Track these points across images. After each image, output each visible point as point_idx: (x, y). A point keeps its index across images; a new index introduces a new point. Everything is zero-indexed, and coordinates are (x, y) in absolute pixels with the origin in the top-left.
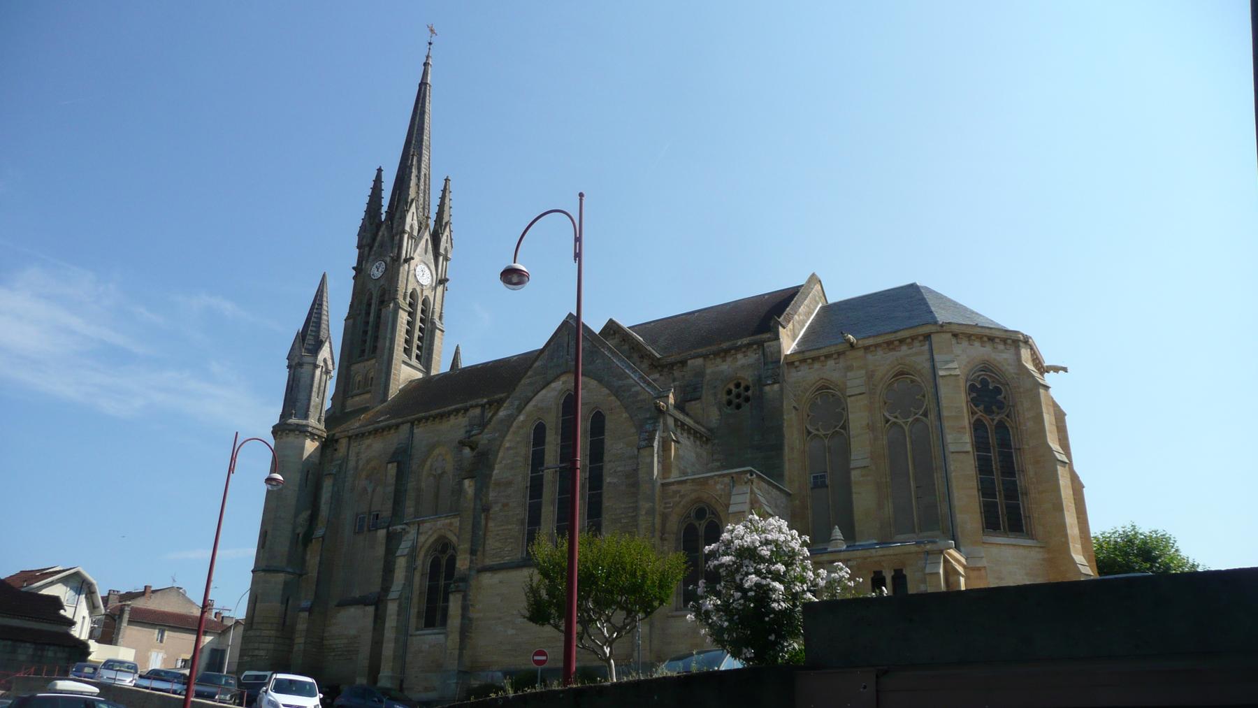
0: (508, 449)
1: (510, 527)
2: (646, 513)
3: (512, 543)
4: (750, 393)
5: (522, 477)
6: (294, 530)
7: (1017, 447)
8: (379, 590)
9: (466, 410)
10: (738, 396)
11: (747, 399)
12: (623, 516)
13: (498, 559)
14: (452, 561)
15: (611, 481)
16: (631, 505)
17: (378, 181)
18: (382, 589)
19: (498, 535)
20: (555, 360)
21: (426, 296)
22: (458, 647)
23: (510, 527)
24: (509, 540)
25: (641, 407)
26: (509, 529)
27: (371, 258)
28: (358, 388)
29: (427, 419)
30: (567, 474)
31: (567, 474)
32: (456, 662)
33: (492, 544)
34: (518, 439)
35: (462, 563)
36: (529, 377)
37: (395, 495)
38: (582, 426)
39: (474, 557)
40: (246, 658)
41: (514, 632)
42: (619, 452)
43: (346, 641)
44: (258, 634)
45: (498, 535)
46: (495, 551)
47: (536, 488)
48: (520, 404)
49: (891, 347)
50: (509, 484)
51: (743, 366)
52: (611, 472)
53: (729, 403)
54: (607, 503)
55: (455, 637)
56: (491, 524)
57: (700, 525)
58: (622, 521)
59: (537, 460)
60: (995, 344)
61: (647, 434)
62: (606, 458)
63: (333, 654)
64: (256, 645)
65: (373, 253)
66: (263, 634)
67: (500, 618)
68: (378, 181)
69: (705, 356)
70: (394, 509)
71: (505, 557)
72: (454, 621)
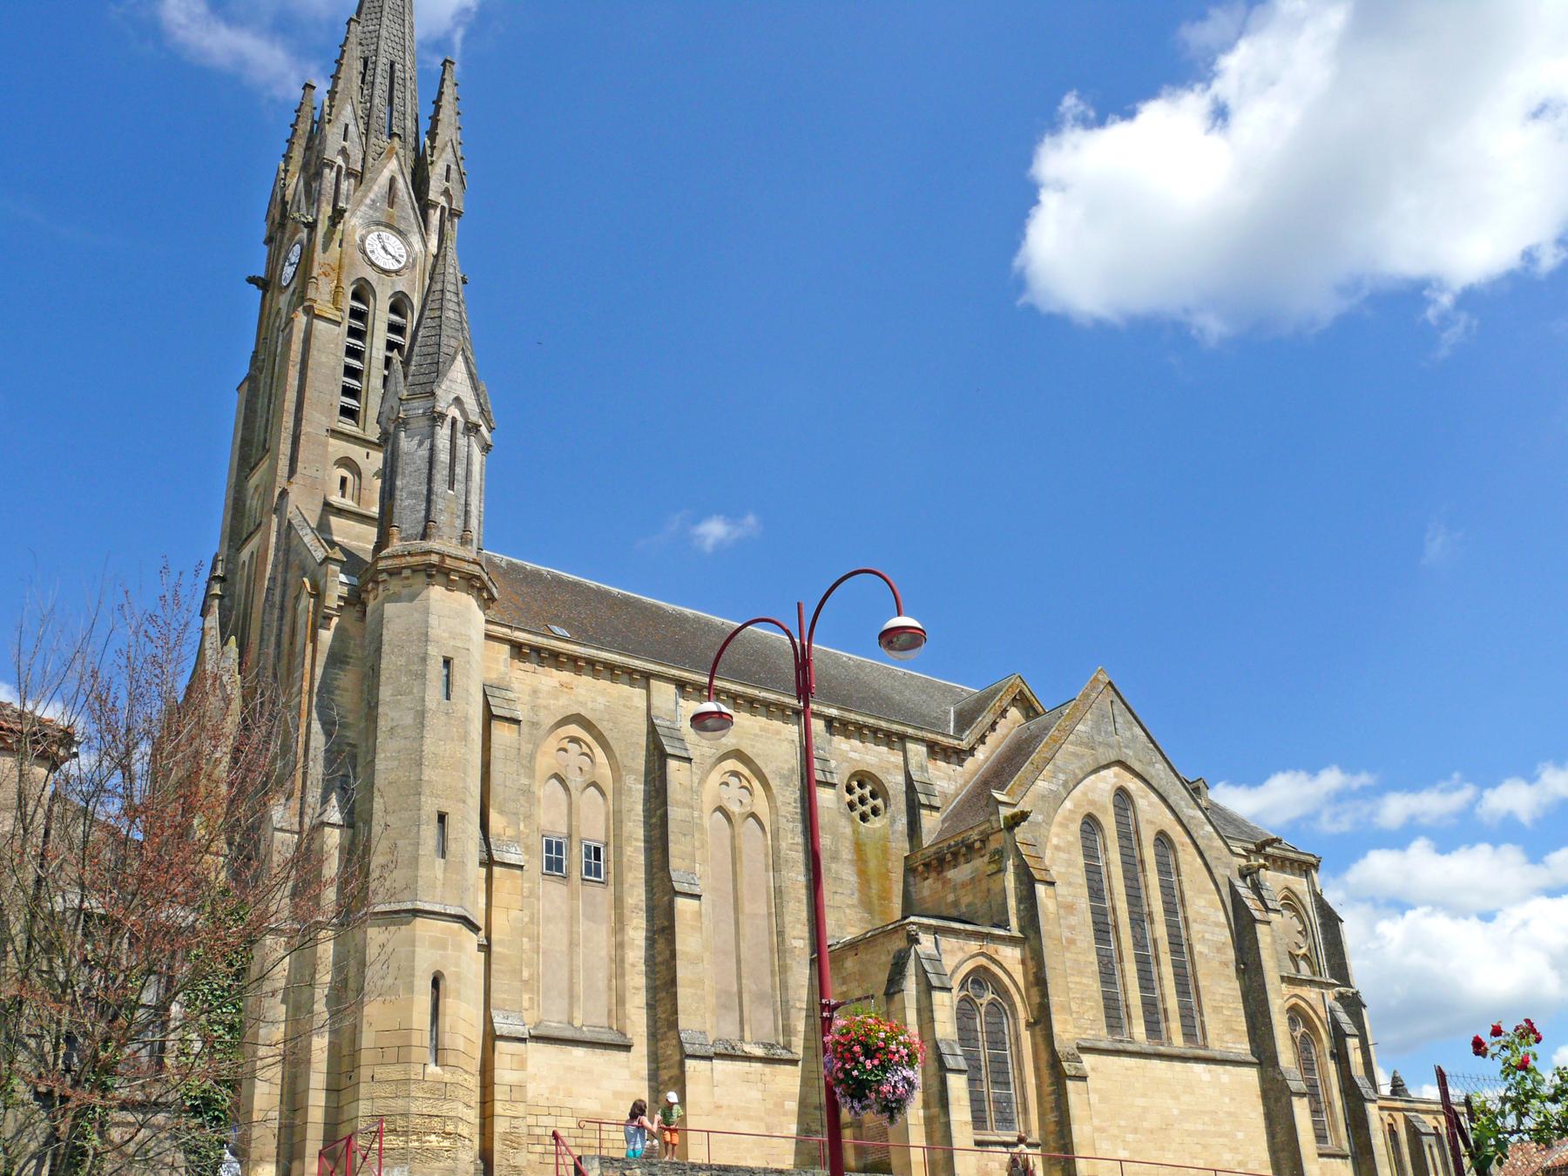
3: (1092, 1008)
11: (875, 811)
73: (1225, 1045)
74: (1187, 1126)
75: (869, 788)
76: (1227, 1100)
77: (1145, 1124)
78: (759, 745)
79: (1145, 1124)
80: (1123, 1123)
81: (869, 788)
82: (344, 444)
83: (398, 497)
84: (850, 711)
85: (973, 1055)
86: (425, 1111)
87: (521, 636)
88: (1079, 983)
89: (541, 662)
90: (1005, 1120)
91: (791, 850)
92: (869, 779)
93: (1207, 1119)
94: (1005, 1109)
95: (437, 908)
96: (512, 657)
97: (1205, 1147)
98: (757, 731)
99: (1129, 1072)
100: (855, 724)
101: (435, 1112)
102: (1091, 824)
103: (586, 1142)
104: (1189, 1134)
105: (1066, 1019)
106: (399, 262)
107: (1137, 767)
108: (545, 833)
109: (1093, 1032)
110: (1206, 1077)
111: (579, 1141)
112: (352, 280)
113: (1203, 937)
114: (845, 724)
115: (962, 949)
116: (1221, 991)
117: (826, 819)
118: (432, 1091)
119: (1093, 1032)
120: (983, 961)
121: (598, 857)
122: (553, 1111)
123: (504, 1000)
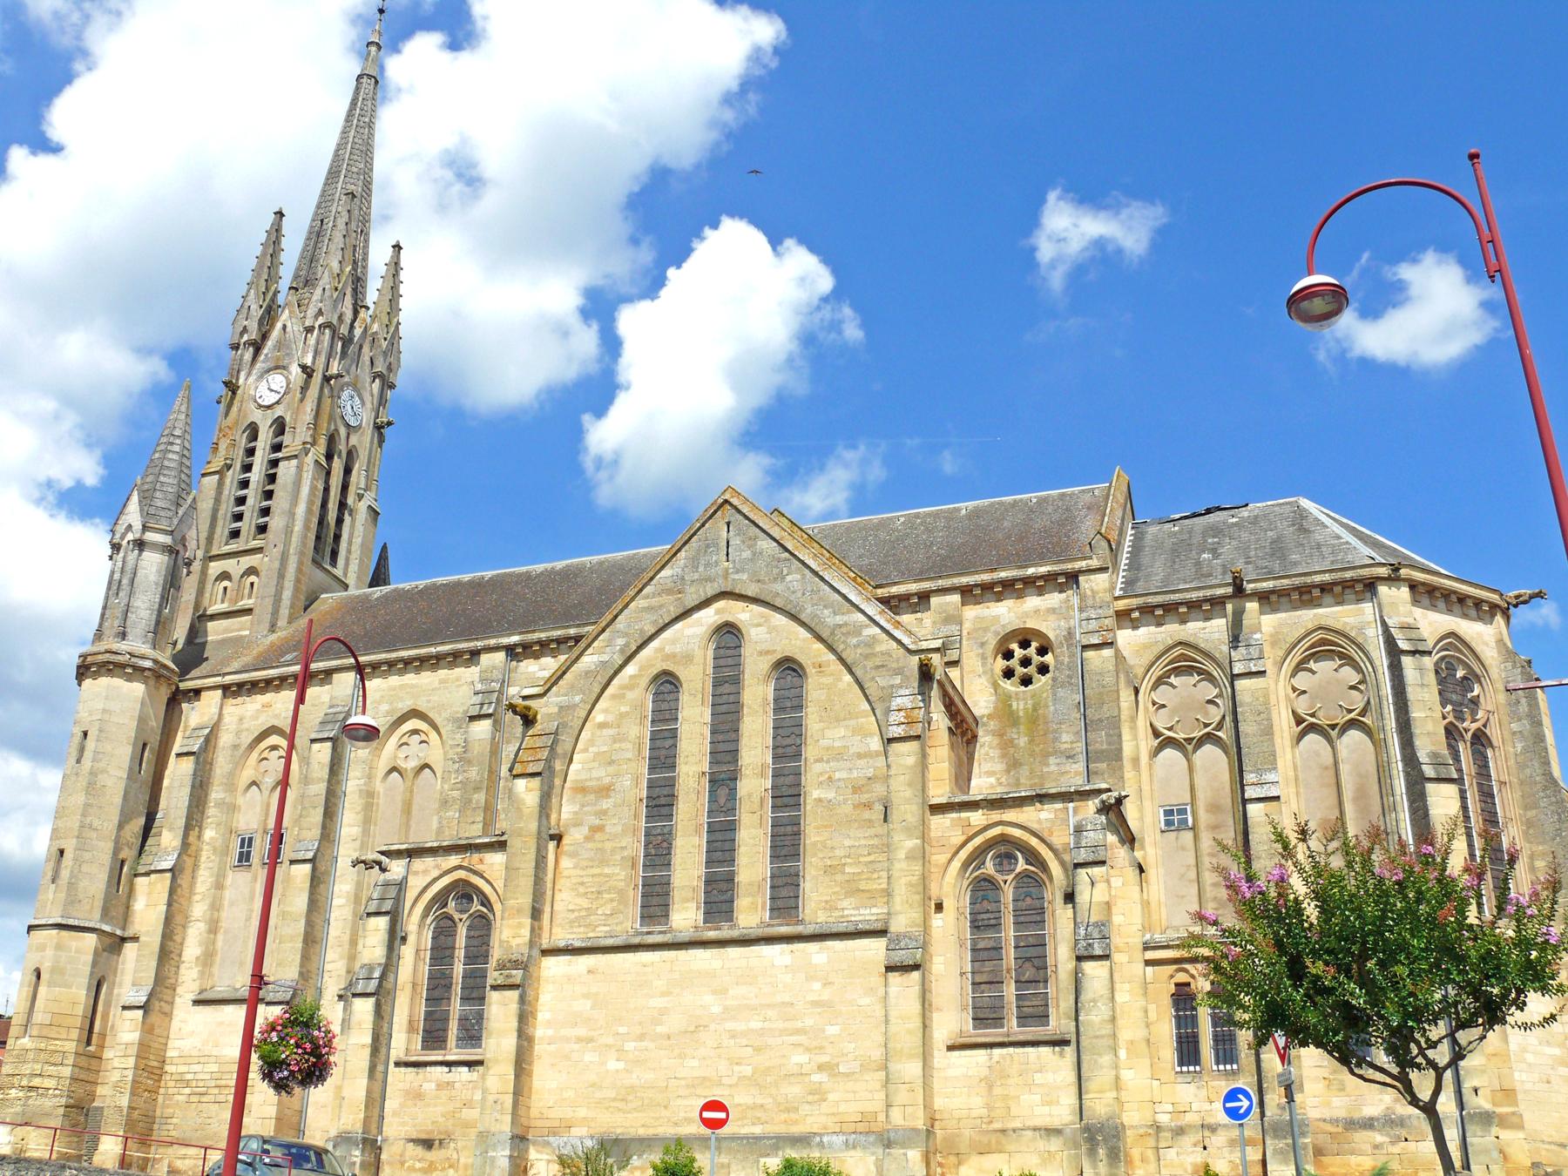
0: (602, 726)
1: (607, 871)
2: (906, 858)
3: (612, 900)
4: (1048, 658)
5: (633, 781)
6: (116, 852)
7: (1502, 779)
8: (296, 975)
9: (475, 654)
10: (1026, 662)
11: (1043, 669)
12: (849, 860)
13: (582, 929)
14: (482, 927)
15: (822, 796)
16: (863, 842)
17: (276, 234)
18: (301, 974)
19: (582, 884)
20: (701, 569)
21: (354, 446)
22: (511, 1090)
23: (607, 871)
24: (606, 896)
25: (883, 666)
26: (607, 875)
27: (259, 365)
28: (223, 602)
29: (391, 664)
30: (724, 776)
31: (724, 776)
32: (509, 1118)
33: (565, 900)
34: (623, 709)
35: (510, 934)
36: (647, 597)
37: (327, 800)
38: (757, 694)
39: (536, 923)
40: (13, 1091)
41: (621, 1065)
42: (837, 744)
43: (214, 1068)
44: (43, 1046)
45: (582, 884)
46: (576, 914)
47: (660, 802)
48: (627, 645)
49: (1305, 597)
50: (605, 791)
51: (1037, 611)
52: (821, 779)
53: (1008, 674)
54: (813, 834)
55: (499, 1075)
56: (566, 863)
57: (1005, 882)
58: (847, 870)
59: (663, 755)
60: (1465, 609)
61: (902, 713)
62: (810, 752)
63: (187, 1091)
64: (38, 1067)
65: (262, 357)
66: (50, 1048)
67: (591, 1040)
68: (276, 234)
69: (967, 593)
70: (324, 827)
71: (596, 926)
72: (499, 1041)
73: (837, 914)
74: (729, 1025)
75: (1015, 646)
76: (817, 986)
77: (659, 1029)
78: (436, 698)
79: (659, 1029)
80: (622, 1030)
81: (1034, 645)
82: (248, 558)
83: (158, 596)
84: (534, 631)
85: (444, 974)
86: (11, 1072)
87: (965, 580)
88: (600, 875)
89: (250, 693)
90: (471, 1038)
91: (452, 790)
92: (1033, 634)
93: (770, 1013)
94: (473, 1025)
95: (43, 922)
96: (331, 683)
97: (758, 1050)
98: (436, 684)
99: (650, 969)
100: (540, 643)
101: (17, 1072)
102: (666, 684)
103: (223, 1083)
104: (733, 1035)
105: (519, 923)
106: (279, 393)
107: (751, 590)
108: (239, 833)
109: (607, 928)
110: (717, 964)
111: (219, 1082)
112: (270, 422)
113: (830, 778)
114: (526, 646)
115: (437, 866)
116: (847, 843)
117: (476, 752)
118: (18, 1056)
119: (607, 928)
120: (461, 874)
121: (250, 845)
122: (202, 1060)
123: (141, 978)
